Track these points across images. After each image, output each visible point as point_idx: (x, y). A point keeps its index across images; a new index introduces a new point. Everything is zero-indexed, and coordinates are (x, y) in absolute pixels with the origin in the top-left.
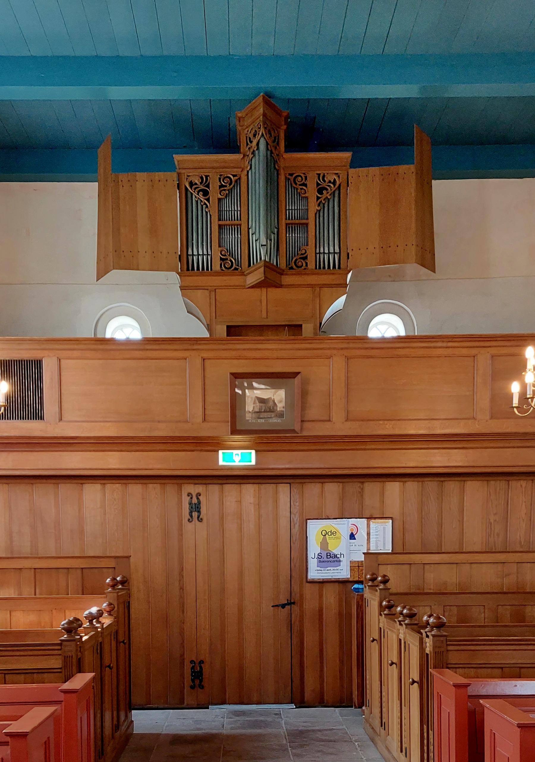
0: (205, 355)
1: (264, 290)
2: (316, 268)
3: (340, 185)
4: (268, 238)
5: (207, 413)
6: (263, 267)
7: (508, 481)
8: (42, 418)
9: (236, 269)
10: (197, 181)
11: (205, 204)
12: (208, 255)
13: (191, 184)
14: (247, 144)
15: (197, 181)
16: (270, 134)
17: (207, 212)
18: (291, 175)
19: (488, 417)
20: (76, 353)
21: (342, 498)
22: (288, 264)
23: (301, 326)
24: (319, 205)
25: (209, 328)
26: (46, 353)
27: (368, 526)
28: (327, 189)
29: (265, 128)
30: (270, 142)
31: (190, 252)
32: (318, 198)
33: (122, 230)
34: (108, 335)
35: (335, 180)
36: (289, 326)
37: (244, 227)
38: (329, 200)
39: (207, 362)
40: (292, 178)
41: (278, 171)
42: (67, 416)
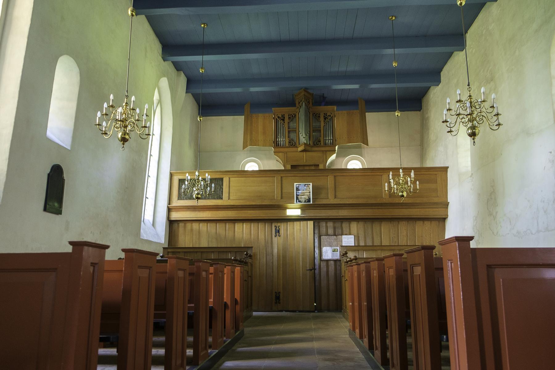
0: (282, 175)
1: (305, 153)
2: (324, 144)
3: (332, 117)
4: (306, 135)
5: (283, 196)
6: (304, 145)
7: (399, 221)
8: (222, 199)
9: (294, 145)
10: (280, 116)
11: (283, 124)
12: (284, 141)
13: (278, 117)
14: (299, 104)
15: (280, 116)
16: (307, 101)
17: (284, 127)
18: (314, 114)
19: (388, 197)
20: (235, 176)
21: (335, 228)
22: (314, 143)
23: (319, 165)
24: (325, 123)
25: (284, 166)
26: (224, 176)
27: (373, 242)
28: (327, 118)
29: (305, 99)
30: (306, 103)
31: (278, 140)
32: (324, 121)
33: (253, 133)
34: (246, 169)
35: (330, 115)
36: (314, 165)
37: (297, 131)
38: (328, 122)
39: (283, 178)
40: (315, 115)
41: (309, 112)
42: (231, 198)
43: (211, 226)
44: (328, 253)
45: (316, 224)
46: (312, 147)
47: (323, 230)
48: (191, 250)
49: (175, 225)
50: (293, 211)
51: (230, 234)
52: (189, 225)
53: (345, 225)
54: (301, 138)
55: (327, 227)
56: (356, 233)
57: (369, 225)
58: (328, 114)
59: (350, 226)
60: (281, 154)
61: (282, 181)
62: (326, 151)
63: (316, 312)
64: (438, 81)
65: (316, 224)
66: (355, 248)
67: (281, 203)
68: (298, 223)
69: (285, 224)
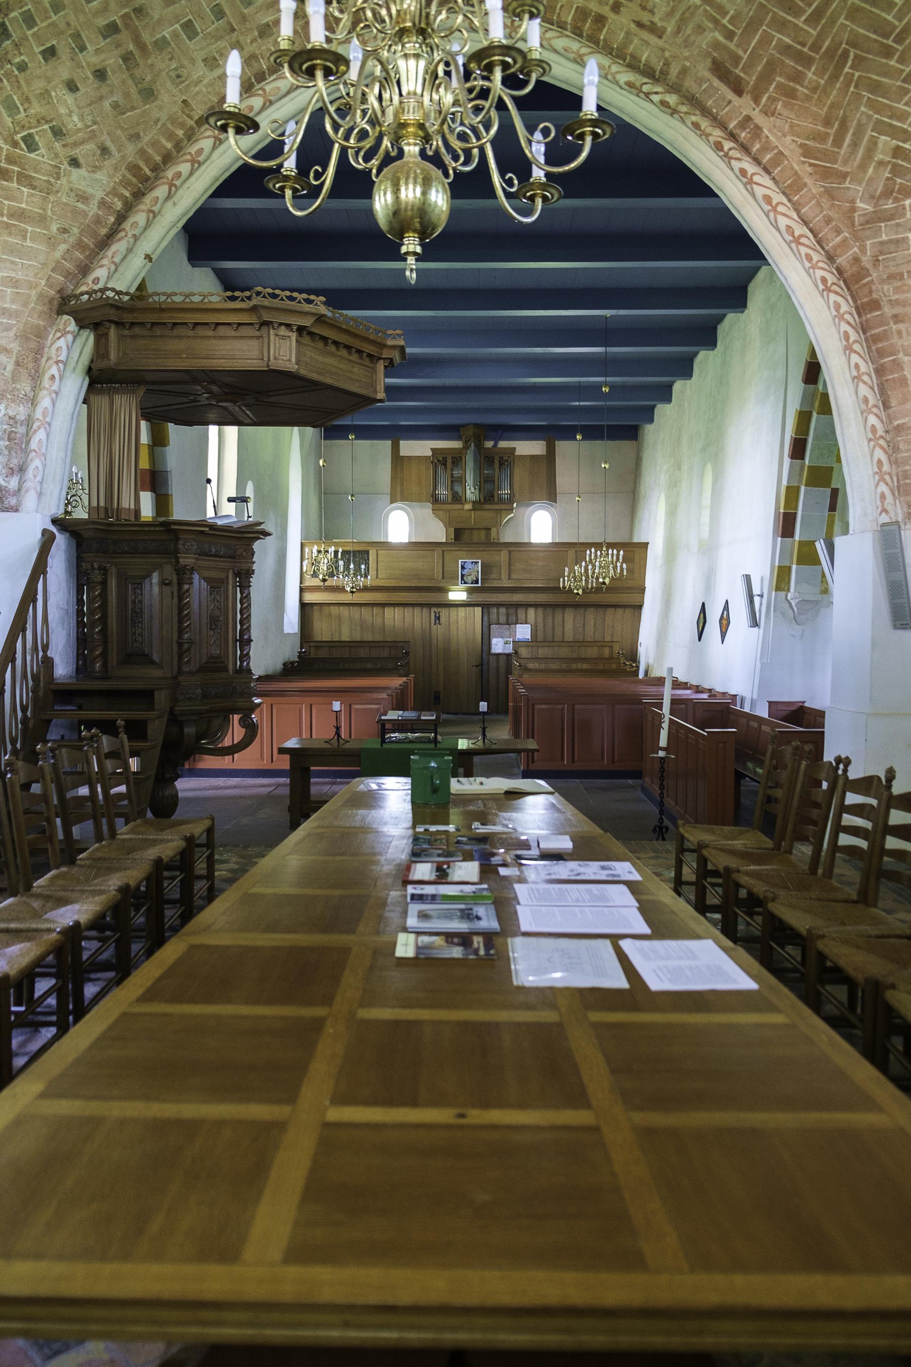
4: (475, 489)
13: (439, 461)
21: (508, 615)
22: (485, 499)
42: (380, 576)
43: (355, 611)
44: (499, 645)
45: (485, 610)
46: (483, 504)
47: (494, 616)
48: (338, 644)
49: (308, 608)
50: (457, 595)
51: (378, 621)
52: (326, 608)
53: (521, 612)
54: (468, 492)
55: (498, 613)
56: (533, 621)
57: (549, 611)
58: (505, 458)
59: (526, 614)
60: (441, 512)
61: (443, 556)
62: (501, 510)
63: (831, 961)
64: (651, 420)
65: (485, 610)
66: (532, 644)
67: (441, 585)
68: (463, 609)
69: (447, 609)
